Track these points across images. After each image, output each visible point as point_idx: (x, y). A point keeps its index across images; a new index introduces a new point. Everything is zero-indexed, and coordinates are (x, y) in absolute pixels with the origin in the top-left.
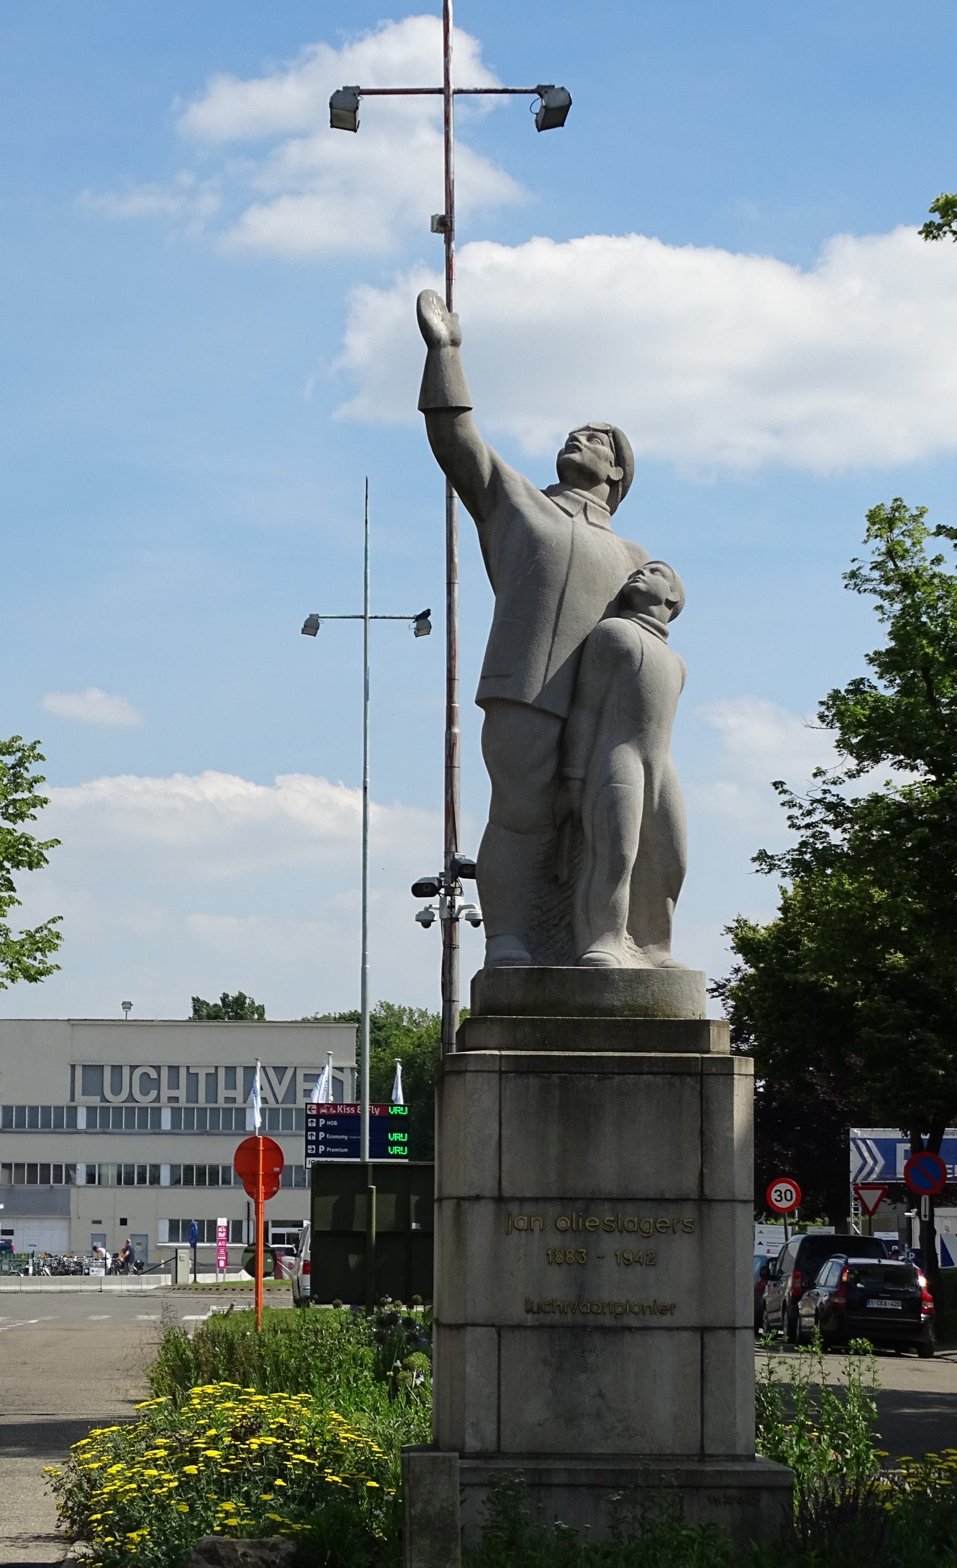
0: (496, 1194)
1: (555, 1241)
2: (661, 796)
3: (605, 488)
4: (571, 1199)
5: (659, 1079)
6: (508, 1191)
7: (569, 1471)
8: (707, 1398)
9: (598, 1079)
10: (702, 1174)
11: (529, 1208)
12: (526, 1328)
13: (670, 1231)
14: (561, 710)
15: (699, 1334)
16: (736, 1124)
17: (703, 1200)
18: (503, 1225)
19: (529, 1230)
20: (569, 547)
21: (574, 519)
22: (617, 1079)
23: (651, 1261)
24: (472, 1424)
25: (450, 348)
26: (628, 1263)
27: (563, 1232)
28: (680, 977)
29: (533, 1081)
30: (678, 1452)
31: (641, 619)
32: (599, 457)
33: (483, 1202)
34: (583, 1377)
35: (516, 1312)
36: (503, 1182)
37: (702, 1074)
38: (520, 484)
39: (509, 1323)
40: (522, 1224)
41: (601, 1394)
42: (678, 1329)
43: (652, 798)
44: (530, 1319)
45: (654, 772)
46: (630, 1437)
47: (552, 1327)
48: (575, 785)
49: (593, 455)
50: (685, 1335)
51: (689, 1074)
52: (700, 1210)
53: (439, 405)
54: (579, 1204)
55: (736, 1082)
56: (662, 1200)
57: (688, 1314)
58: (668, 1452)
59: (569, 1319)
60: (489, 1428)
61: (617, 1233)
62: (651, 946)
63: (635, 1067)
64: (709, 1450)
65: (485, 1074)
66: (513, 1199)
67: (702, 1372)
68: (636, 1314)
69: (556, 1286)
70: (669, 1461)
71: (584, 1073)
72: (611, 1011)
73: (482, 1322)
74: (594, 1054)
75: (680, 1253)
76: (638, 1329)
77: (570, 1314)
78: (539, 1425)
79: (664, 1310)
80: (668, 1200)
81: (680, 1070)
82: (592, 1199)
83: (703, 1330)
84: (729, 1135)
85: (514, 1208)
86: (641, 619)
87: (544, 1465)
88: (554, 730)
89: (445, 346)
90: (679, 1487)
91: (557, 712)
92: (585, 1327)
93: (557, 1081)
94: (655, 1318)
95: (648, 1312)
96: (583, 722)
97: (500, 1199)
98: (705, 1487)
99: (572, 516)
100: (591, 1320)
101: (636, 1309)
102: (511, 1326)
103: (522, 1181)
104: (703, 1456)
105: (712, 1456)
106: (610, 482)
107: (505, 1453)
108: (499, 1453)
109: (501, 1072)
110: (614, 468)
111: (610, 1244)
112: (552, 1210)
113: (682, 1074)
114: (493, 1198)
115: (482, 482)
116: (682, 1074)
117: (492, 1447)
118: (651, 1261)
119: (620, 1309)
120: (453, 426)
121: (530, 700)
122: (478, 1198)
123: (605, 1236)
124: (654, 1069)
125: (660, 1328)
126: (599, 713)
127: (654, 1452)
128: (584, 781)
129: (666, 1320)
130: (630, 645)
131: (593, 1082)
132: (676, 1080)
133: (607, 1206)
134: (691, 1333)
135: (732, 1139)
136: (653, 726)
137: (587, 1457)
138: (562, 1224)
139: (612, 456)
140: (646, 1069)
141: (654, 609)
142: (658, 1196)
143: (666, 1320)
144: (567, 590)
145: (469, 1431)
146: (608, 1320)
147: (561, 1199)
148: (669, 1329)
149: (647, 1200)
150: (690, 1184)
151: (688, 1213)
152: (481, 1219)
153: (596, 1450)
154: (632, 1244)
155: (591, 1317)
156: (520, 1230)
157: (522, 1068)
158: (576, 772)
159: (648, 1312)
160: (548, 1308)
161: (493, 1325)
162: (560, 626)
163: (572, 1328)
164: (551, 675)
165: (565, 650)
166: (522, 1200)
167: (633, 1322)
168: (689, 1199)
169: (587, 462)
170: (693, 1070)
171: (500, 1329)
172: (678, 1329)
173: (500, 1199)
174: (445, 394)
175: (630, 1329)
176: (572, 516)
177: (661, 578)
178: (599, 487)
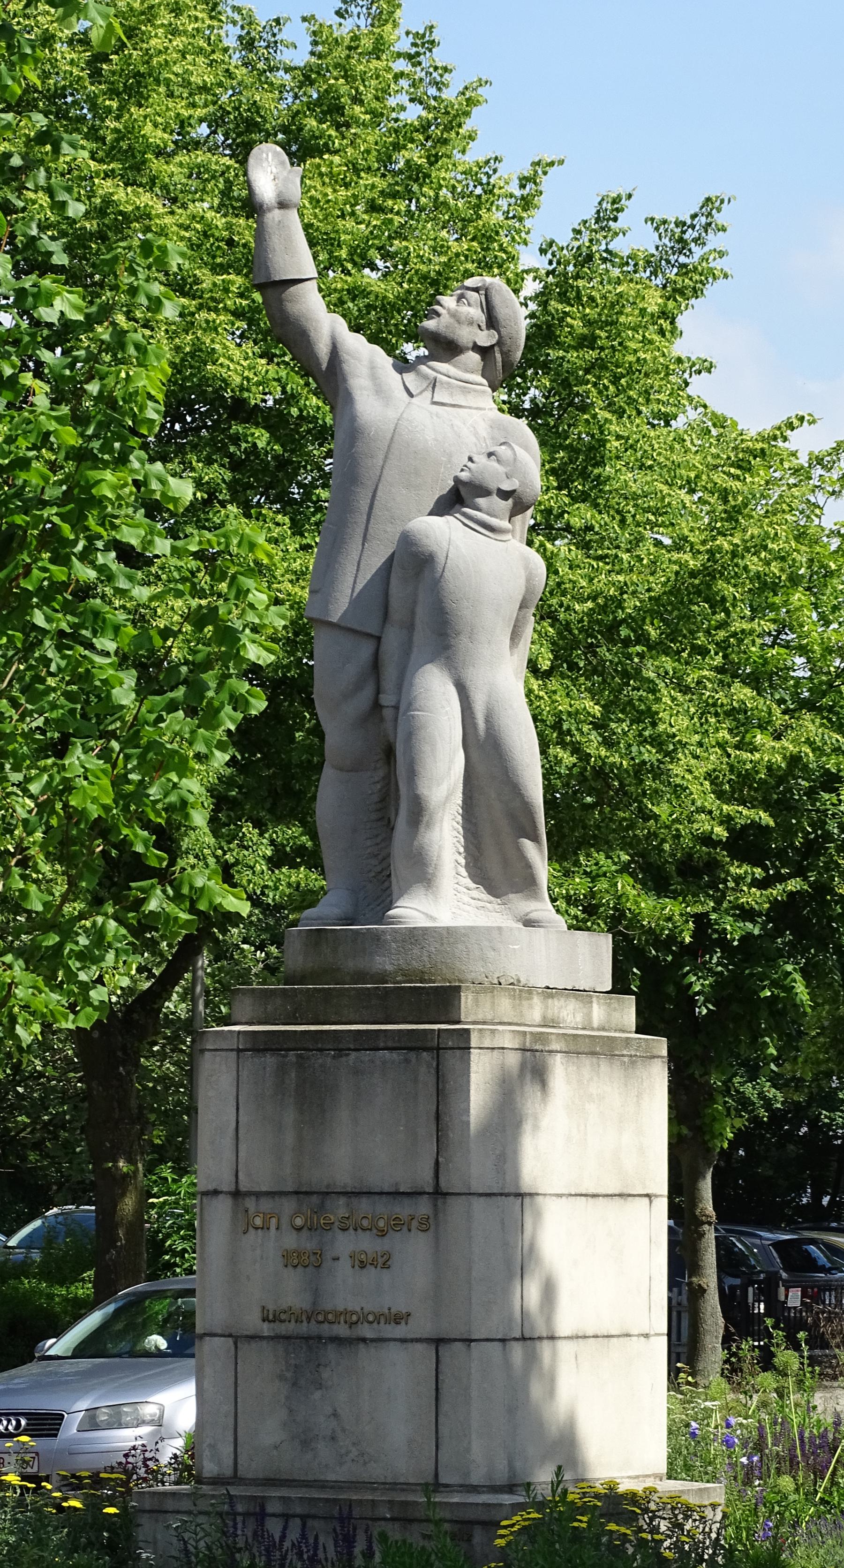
0: (232, 1188)
1: (290, 1241)
2: (488, 719)
3: (474, 358)
4: (306, 1193)
5: (394, 1055)
6: (244, 1186)
7: (282, 1499)
8: (441, 1419)
9: (334, 1057)
10: (437, 1163)
11: (266, 1205)
12: (262, 1338)
13: (405, 1228)
14: (373, 629)
15: (433, 1347)
16: (473, 1105)
17: (438, 1194)
18: (244, 1224)
19: (265, 1227)
20: (389, 436)
21: (414, 400)
22: (353, 1055)
23: (385, 1262)
24: (210, 1445)
25: (277, 212)
26: (363, 1265)
27: (299, 1229)
28: (465, 935)
29: (270, 1060)
30: (411, 1481)
31: (465, 515)
32: (459, 322)
33: (221, 1197)
34: (318, 1395)
35: (253, 1322)
36: (240, 1174)
37: (438, 1049)
38: (365, 363)
39: (246, 1333)
40: (258, 1222)
41: (335, 1415)
42: (412, 1340)
43: (475, 726)
44: (266, 1329)
45: (472, 694)
46: (365, 1463)
47: (287, 1338)
48: (388, 713)
49: (452, 320)
50: (419, 1347)
51: (425, 1049)
52: (435, 1205)
53: (263, 281)
54: (315, 1199)
55: (472, 1057)
56: (396, 1194)
57: (422, 1325)
58: (402, 1480)
59: (304, 1328)
60: (227, 1450)
61: (351, 1231)
62: (511, 896)
63: (367, 1042)
64: (443, 1480)
65: (223, 1053)
66: (249, 1194)
67: (437, 1389)
68: (371, 1323)
69: (292, 1292)
70: (403, 1490)
71: (321, 1050)
72: (382, 977)
73: (219, 1331)
74: (333, 1027)
75: (413, 1251)
76: (373, 1340)
77: (305, 1323)
78: (276, 1447)
79: (398, 1319)
80: (403, 1193)
81: (414, 1044)
82: (327, 1193)
83: (438, 1342)
84: (464, 1118)
85: (250, 1203)
86: (465, 515)
87: (402, 1497)
88: (366, 650)
89: (270, 210)
90: (393, 1519)
91: (369, 631)
92: (320, 1338)
93: (294, 1059)
94: (389, 1327)
95: (382, 1321)
96: (392, 639)
97: (237, 1194)
98: (420, 1521)
99: (411, 395)
100: (326, 1330)
101: (371, 1318)
102: (247, 1337)
103: (259, 1175)
104: (437, 1486)
105: (447, 1486)
106: (476, 348)
107: (241, 1479)
108: (235, 1479)
109: (239, 1051)
110: (486, 332)
111: (345, 1244)
112: (288, 1206)
113: (419, 1049)
114: (230, 1193)
115: (319, 364)
116: (419, 1049)
117: (229, 1472)
118: (385, 1262)
119: (354, 1318)
120: (281, 301)
121: (335, 618)
122: (216, 1193)
123: (341, 1236)
124: (390, 1044)
125: (395, 1340)
126: (410, 627)
127: (389, 1480)
128: (396, 708)
129: (400, 1331)
130: (434, 548)
131: (329, 1060)
132: (412, 1055)
133: (342, 1201)
134: (425, 1345)
135: (468, 1123)
136: (464, 640)
137: (323, 1485)
138: (299, 1222)
139: (482, 318)
140: (382, 1045)
141: (481, 501)
142: (392, 1190)
143: (400, 1331)
144: (380, 487)
145: (207, 1453)
146: (342, 1330)
147: (297, 1193)
148: (403, 1341)
149: (381, 1193)
150: (424, 1177)
151: (424, 1207)
152: (219, 1213)
153: (331, 1477)
154: (367, 1243)
155: (326, 1326)
156: (257, 1229)
157: (259, 1045)
158: (387, 700)
159: (382, 1321)
160: (283, 1316)
161: (230, 1336)
162: (370, 530)
163: (307, 1338)
164: (359, 587)
165: (375, 561)
166: (258, 1195)
167: (367, 1331)
168: (425, 1193)
169: (442, 330)
170: (429, 1044)
171: (237, 1339)
172: (412, 1340)
173: (237, 1194)
174: (267, 268)
175: (364, 1340)
176: (411, 395)
177: (496, 464)
178: (462, 358)
